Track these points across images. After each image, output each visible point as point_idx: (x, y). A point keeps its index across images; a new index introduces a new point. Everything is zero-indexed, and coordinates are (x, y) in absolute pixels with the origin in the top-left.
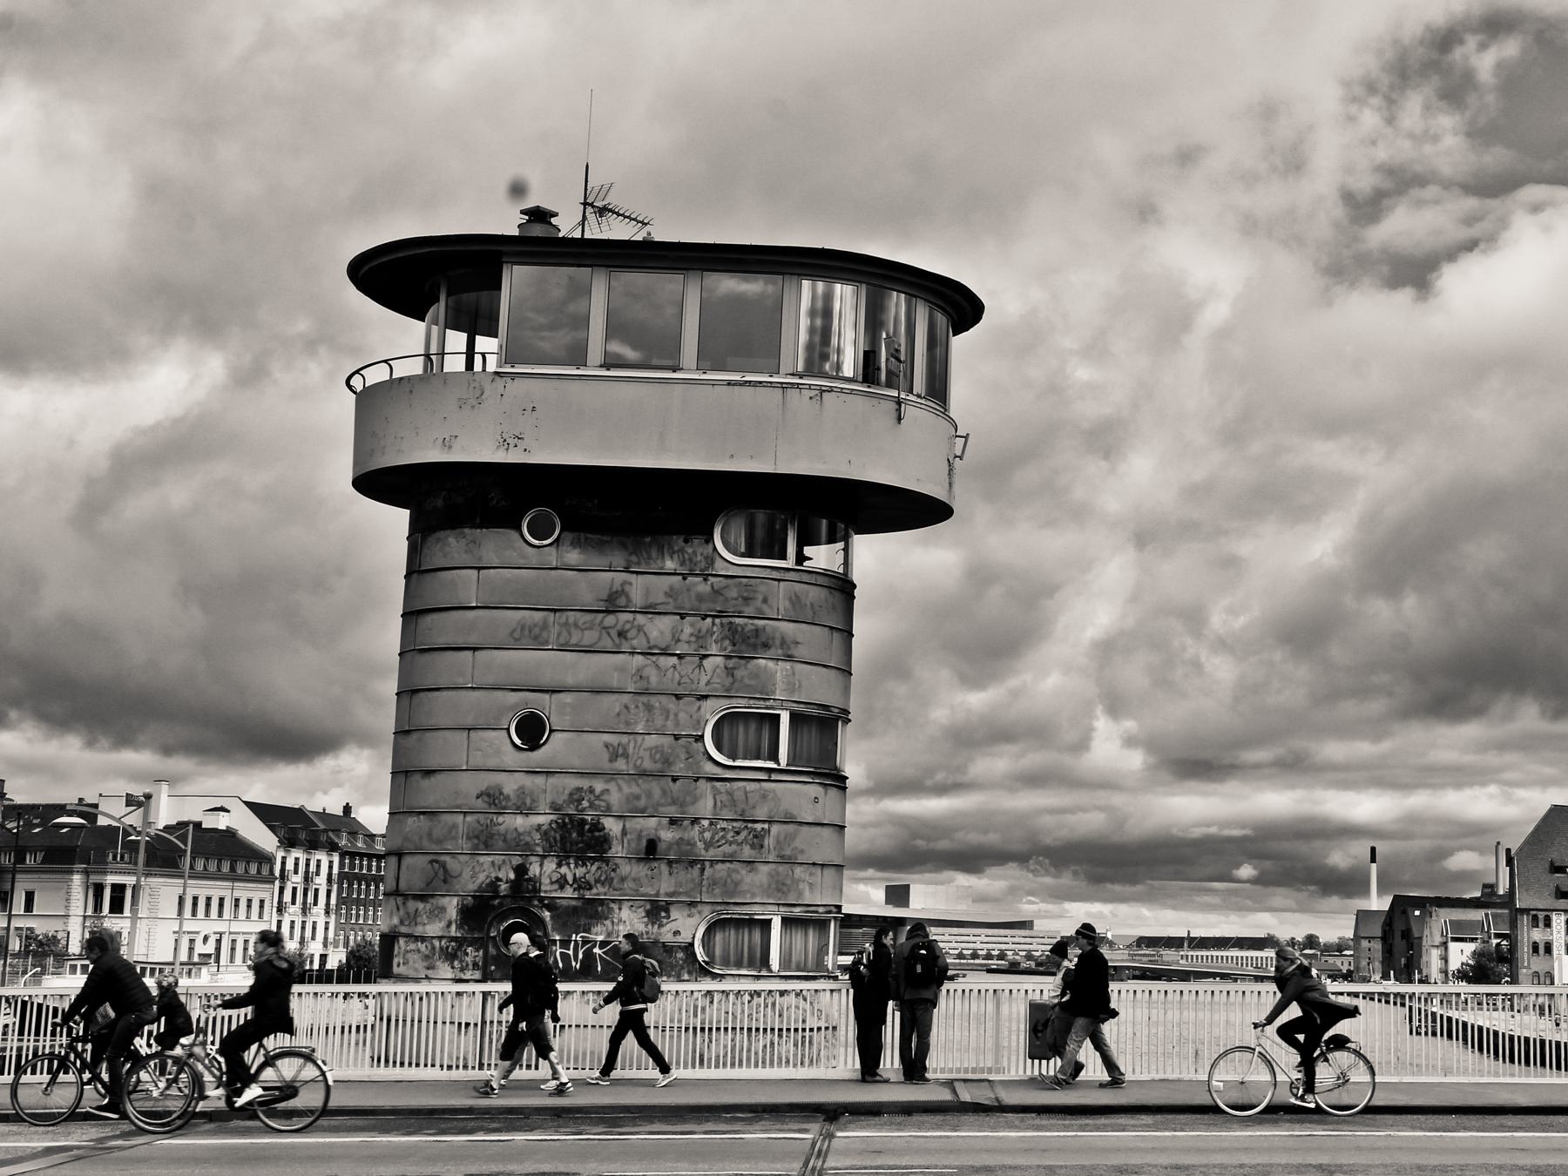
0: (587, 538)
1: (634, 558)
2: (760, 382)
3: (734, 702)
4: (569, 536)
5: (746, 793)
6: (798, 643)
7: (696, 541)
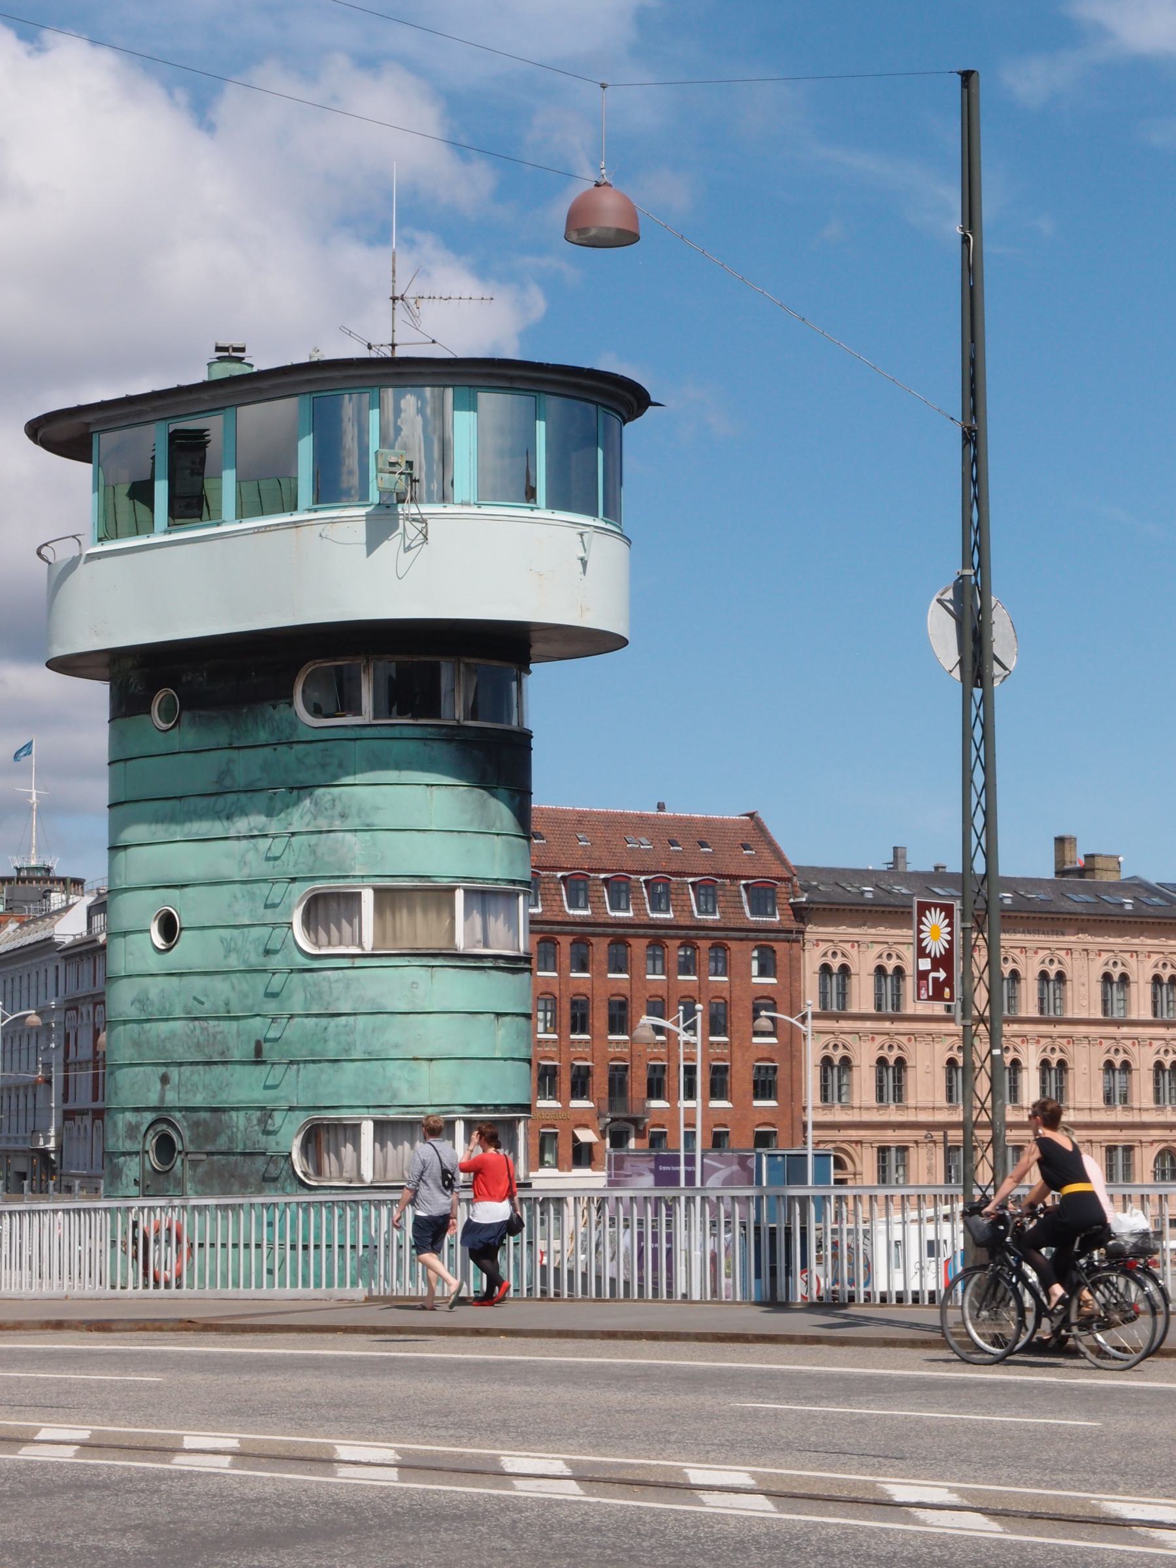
0: (200, 716)
1: (235, 733)
2: (278, 525)
3: (318, 885)
4: (186, 716)
5: (330, 982)
6: (378, 809)
7: (282, 706)
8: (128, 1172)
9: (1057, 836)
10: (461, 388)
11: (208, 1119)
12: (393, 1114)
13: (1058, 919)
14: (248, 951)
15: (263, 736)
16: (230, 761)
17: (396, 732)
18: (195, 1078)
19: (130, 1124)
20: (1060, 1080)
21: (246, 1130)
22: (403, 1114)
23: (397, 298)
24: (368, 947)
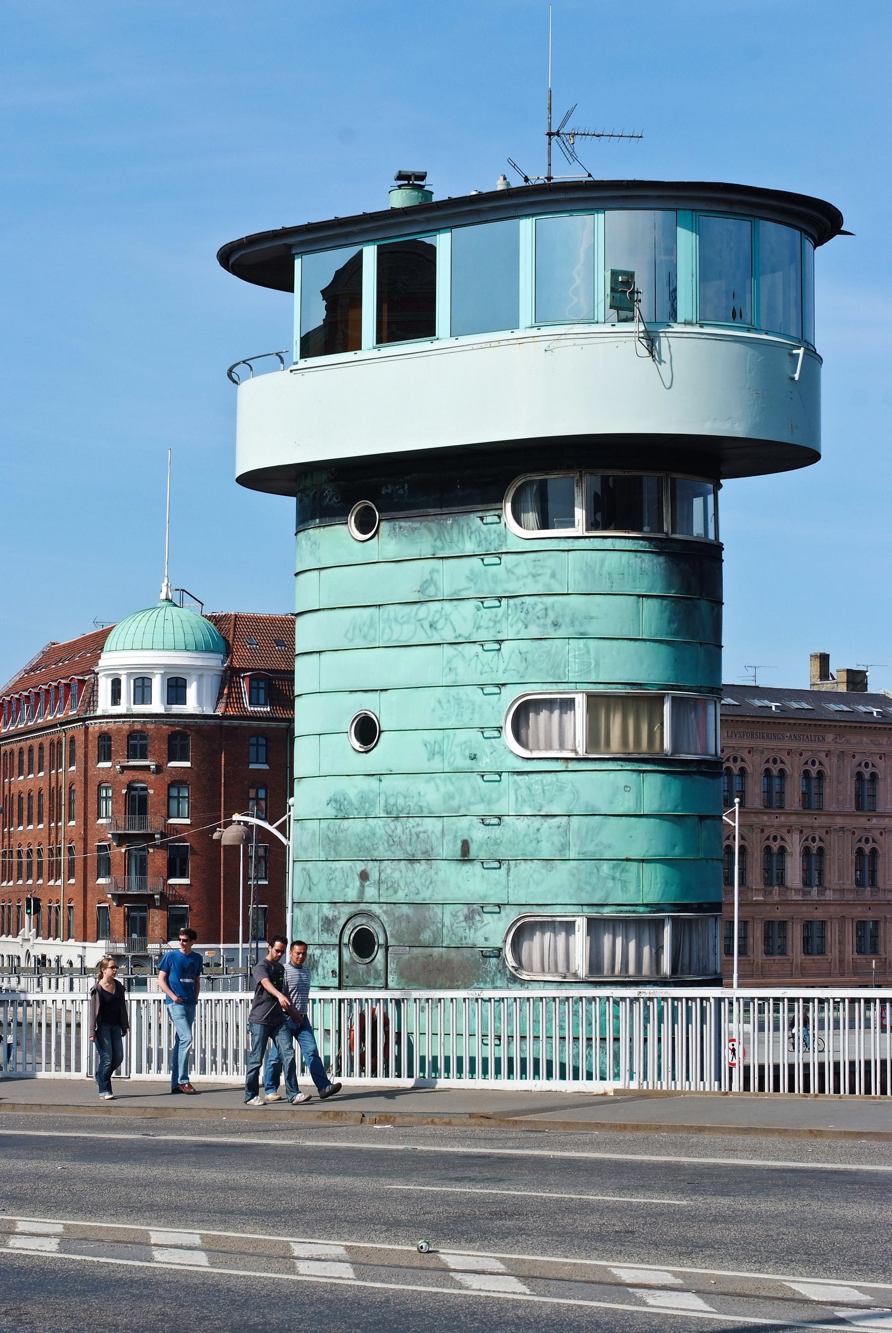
0: (400, 528)
1: (439, 544)
4: (385, 527)
8: (325, 964)
9: (812, 653)
10: (683, 212)
11: (411, 915)
12: (607, 912)
13: (820, 725)
14: (454, 754)
15: (469, 547)
16: (433, 571)
17: (608, 544)
18: (397, 875)
19: (327, 918)
20: (821, 863)
21: (452, 926)
22: (617, 912)
23: (553, 134)
24: (581, 753)
